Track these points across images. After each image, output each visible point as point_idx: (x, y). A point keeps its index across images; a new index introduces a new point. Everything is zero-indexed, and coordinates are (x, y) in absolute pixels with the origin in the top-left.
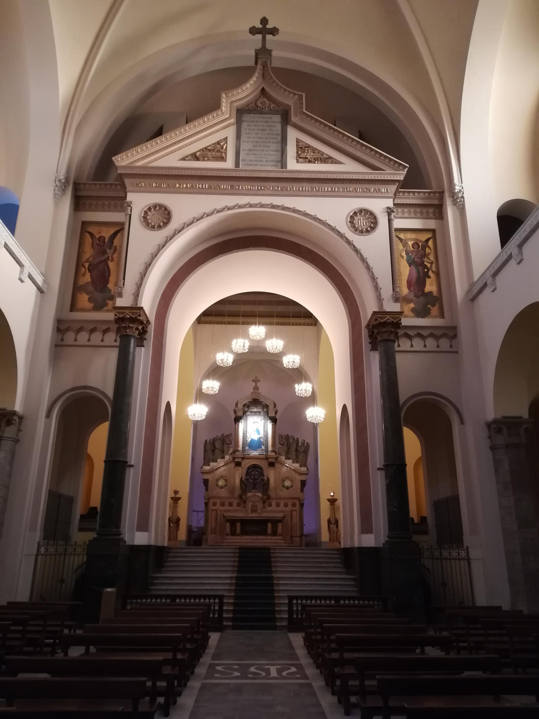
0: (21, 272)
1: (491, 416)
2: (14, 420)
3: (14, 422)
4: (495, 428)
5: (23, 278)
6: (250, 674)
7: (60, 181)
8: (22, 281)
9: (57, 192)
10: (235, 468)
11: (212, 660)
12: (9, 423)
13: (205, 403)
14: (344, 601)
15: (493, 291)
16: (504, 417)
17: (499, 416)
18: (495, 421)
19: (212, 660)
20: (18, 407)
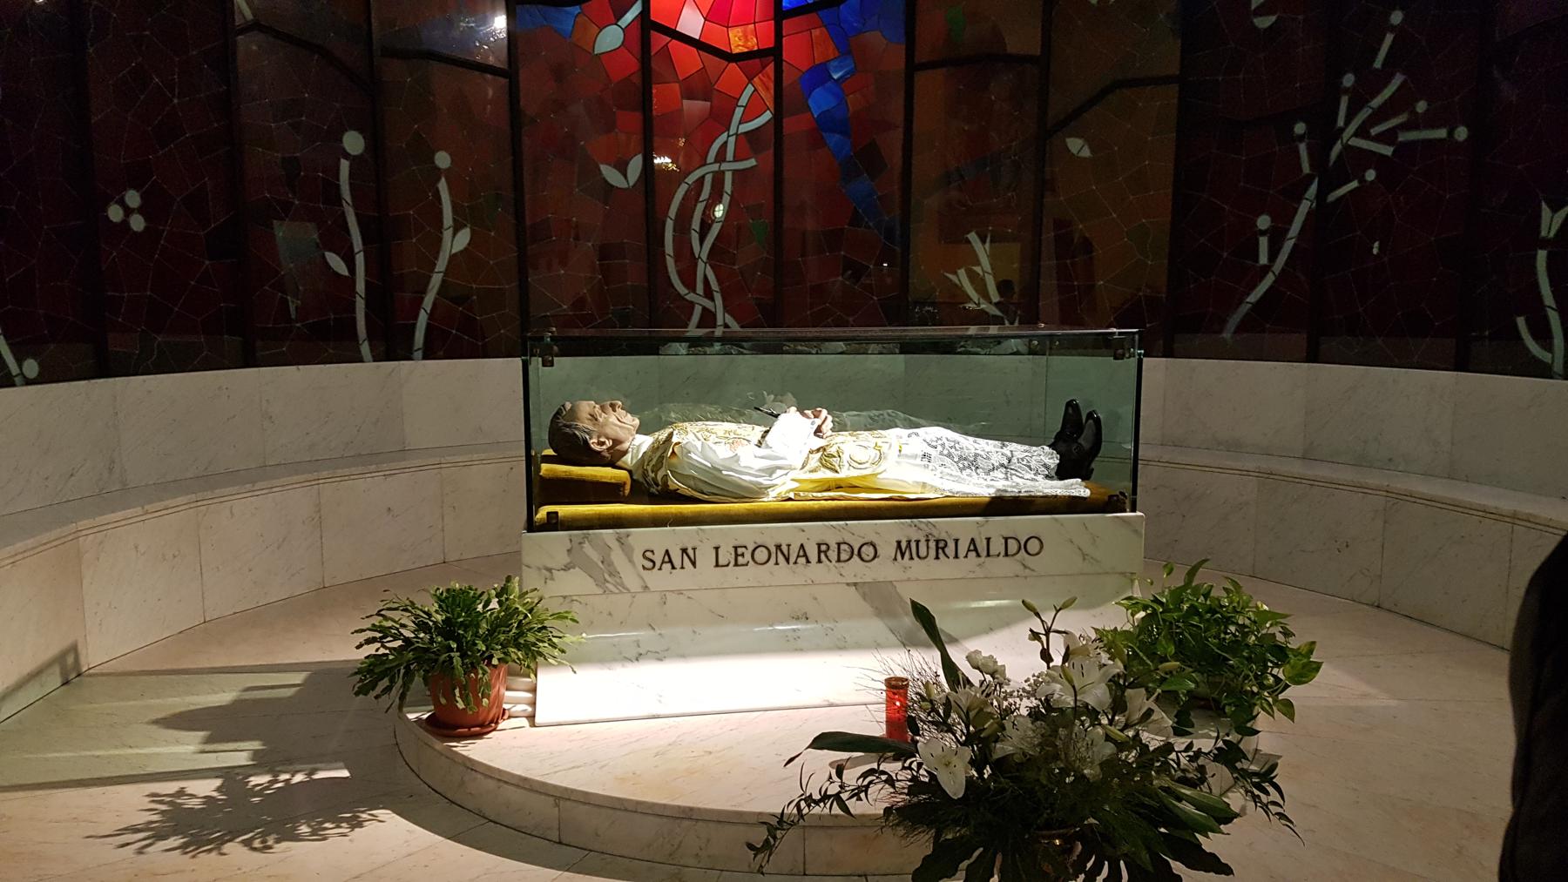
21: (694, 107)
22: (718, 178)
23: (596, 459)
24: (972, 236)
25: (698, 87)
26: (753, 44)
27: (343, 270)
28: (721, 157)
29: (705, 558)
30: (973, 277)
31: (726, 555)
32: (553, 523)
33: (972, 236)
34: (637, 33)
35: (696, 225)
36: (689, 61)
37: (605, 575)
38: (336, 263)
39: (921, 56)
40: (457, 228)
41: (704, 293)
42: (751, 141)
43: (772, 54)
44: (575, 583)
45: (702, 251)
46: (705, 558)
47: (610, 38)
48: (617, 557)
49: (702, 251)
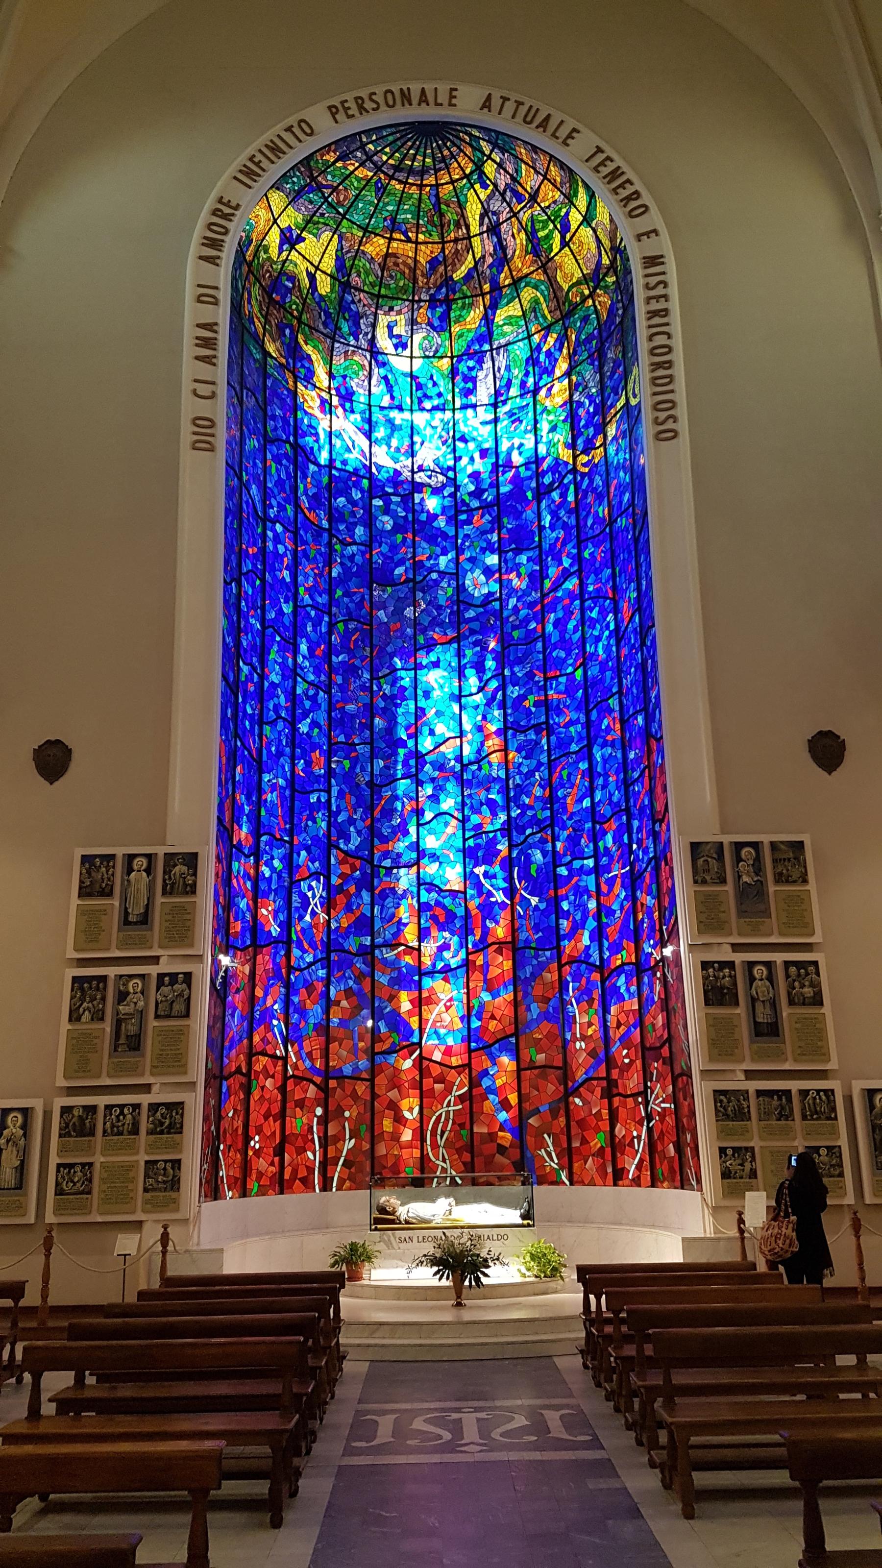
21: (438, 1087)
22: (448, 1112)
23: (388, 1213)
24: (546, 1136)
25: (440, 1079)
26: (460, 1062)
27: (311, 1157)
28: (448, 1105)
29: (415, 1240)
30: (546, 1151)
31: (421, 1239)
32: (376, 1229)
33: (546, 1136)
34: (417, 1062)
35: (439, 1132)
36: (436, 1070)
37: (389, 1244)
38: (310, 1155)
39: (522, 1066)
40: (350, 1139)
41: (443, 1163)
42: (461, 1099)
43: (469, 1065)
44: (381, 1246)
45: (441, 1142)
46: (415, 1240)
47: (408, 1064)
48: (392, 1238)
49: (441, 1142)
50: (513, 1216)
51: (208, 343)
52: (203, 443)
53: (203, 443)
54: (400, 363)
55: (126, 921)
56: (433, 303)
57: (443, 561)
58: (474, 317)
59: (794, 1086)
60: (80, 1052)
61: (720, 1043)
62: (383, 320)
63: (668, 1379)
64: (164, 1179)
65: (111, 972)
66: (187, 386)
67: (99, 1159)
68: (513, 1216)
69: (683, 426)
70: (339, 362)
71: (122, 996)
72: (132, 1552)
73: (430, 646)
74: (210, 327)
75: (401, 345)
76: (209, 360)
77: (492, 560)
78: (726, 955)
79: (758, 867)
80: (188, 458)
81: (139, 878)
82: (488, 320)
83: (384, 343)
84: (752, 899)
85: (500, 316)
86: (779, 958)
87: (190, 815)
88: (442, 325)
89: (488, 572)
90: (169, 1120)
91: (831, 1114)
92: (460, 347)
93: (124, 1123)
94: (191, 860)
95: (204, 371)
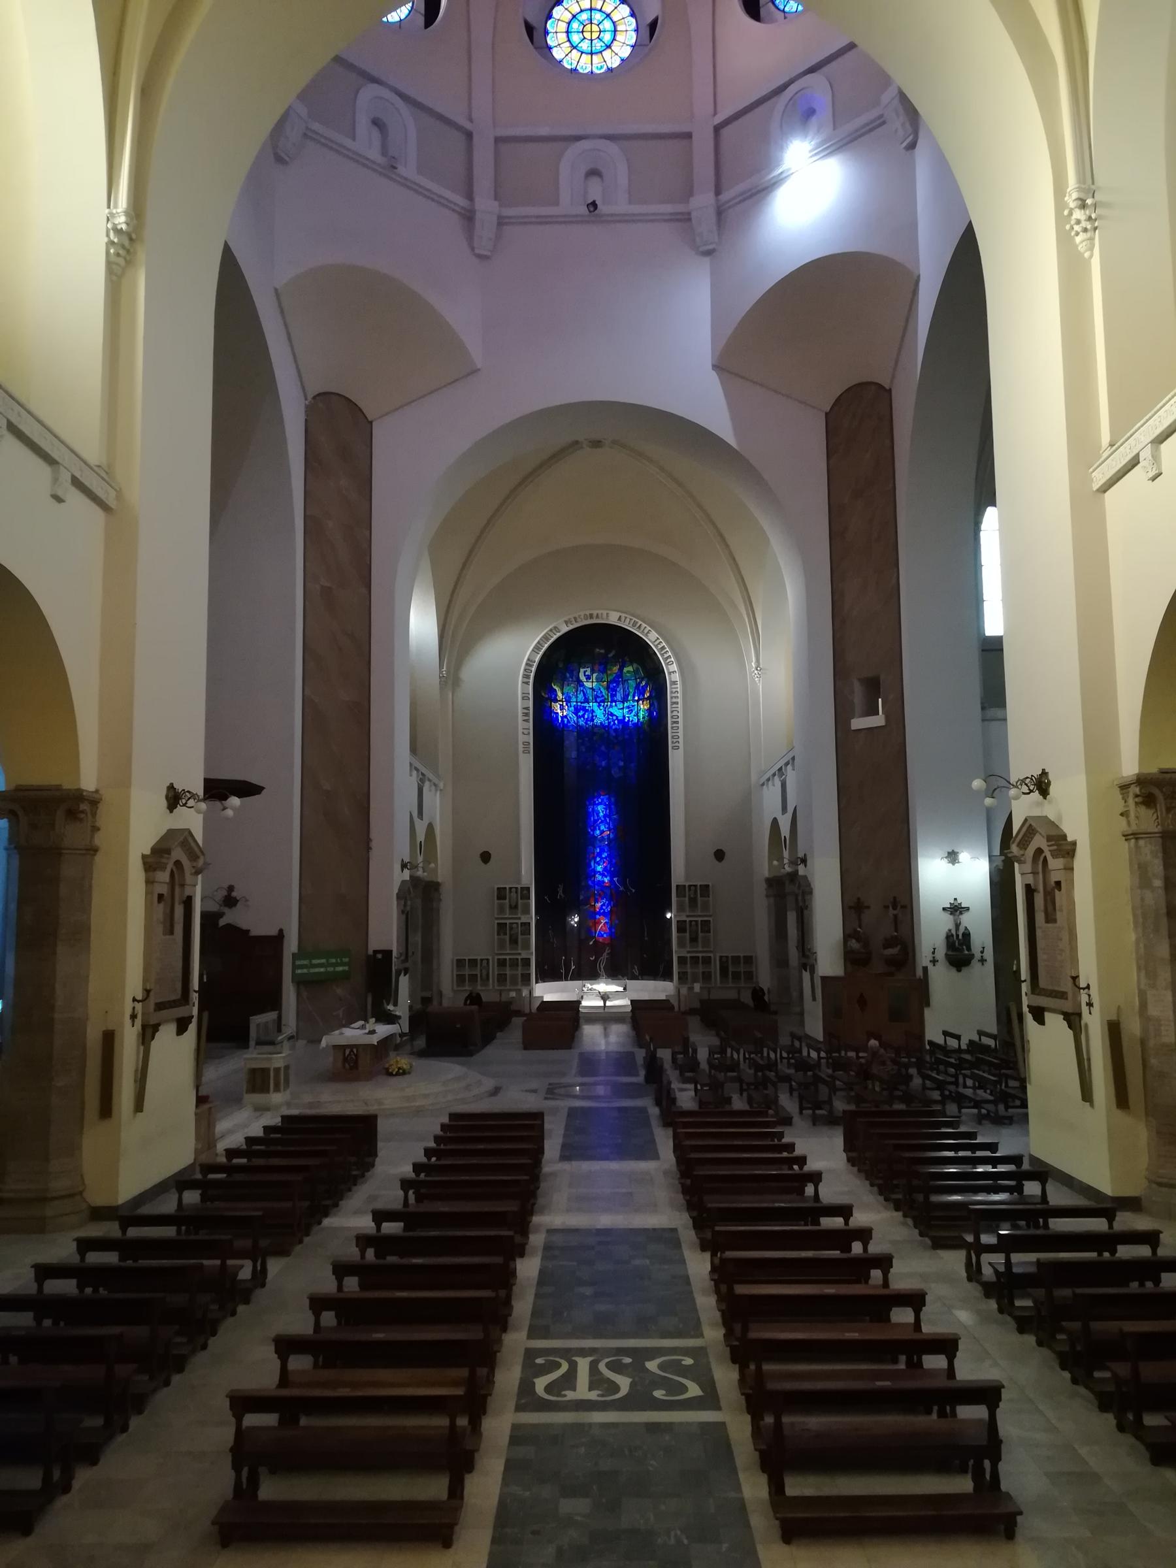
0: (55, 480)
1: (767, 874)
2: (82, 812)
3: (82, 816)
4: (1137, 796)
5: (60, 493)
6: (626, 1365)
7: (118, 232)
8: (59, 499)
9: (113, 259)
10: (134, 1116)
11: (530, 1337)
12: (73, 814)
13: (782, 149)
14: (1142, 1285)
15: (1154, 479)
16: (1164, 772)
17: (1153, 769)
18: (1140, 780)
19: (530, 1337)
20: (88, 781)
50: (621, 989)
51: (527, 715)
52: (526, 752)
53: (526, 752)
54: (588, 685)
55: (511, 907)
56: (600, 664)
57: (604, 763)
58: (616, 669)
59: (700, 955)
60: (502, 945)
61: (681, 944)
62: (582, 670)
63: (977, 1238)
64: (526, 979)
65: (508, 922)
66: (520, 731)
67: (508, 972)
68: (621, 989)
69: (681, 745)
70: (565, 691)
71: (511, 929)
72: (579, 1002)
73: (599, 797)
74: (527, 708)
75: (588, 678)
76: (527, 721)
77: (622, 764)
78: (684, 918)
79: (696, 891)
80: (521, 756)
81: (513, 895)
82: (621, 670)
83: (583, 678)
84: (693, 902)
85: (625, 670)
86: (700, 919)
87: (527, 874)
88: (604, 671)
89: (620, 768)
90: (527, 962)
91: (710, 962)
92: (610, 678)
93: (514, 963)
94: (528, 889)
95: (526, 725)
